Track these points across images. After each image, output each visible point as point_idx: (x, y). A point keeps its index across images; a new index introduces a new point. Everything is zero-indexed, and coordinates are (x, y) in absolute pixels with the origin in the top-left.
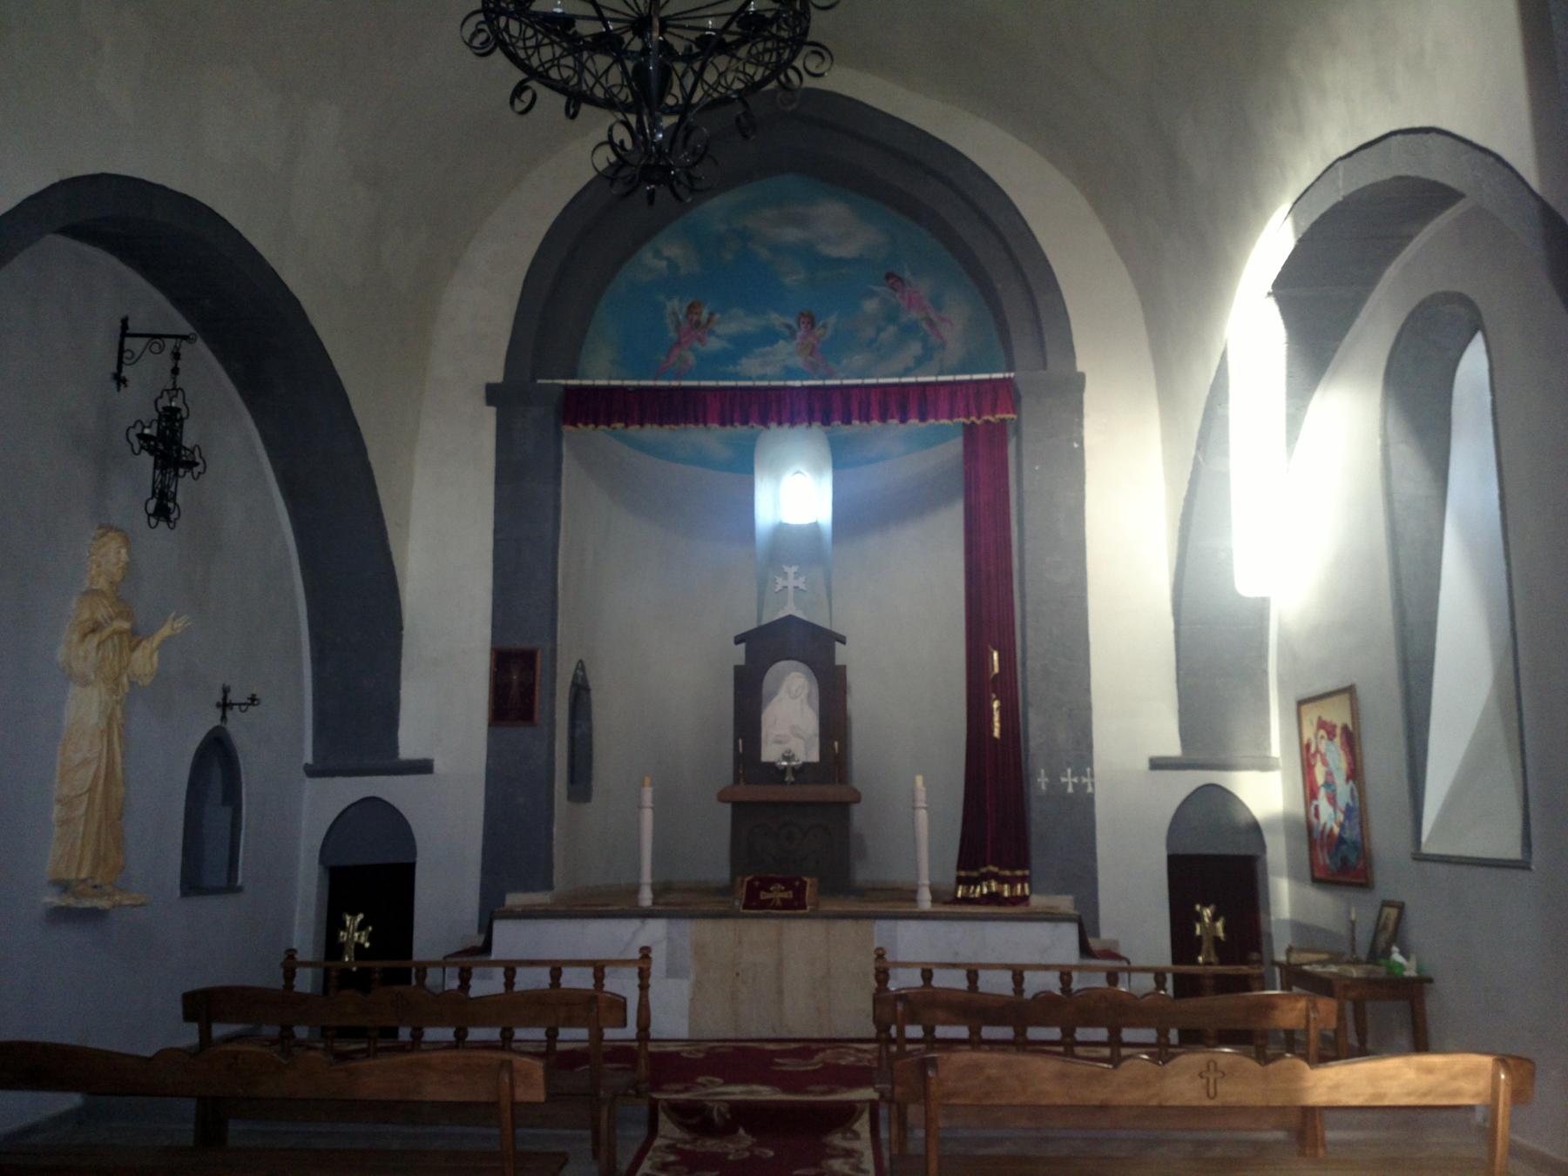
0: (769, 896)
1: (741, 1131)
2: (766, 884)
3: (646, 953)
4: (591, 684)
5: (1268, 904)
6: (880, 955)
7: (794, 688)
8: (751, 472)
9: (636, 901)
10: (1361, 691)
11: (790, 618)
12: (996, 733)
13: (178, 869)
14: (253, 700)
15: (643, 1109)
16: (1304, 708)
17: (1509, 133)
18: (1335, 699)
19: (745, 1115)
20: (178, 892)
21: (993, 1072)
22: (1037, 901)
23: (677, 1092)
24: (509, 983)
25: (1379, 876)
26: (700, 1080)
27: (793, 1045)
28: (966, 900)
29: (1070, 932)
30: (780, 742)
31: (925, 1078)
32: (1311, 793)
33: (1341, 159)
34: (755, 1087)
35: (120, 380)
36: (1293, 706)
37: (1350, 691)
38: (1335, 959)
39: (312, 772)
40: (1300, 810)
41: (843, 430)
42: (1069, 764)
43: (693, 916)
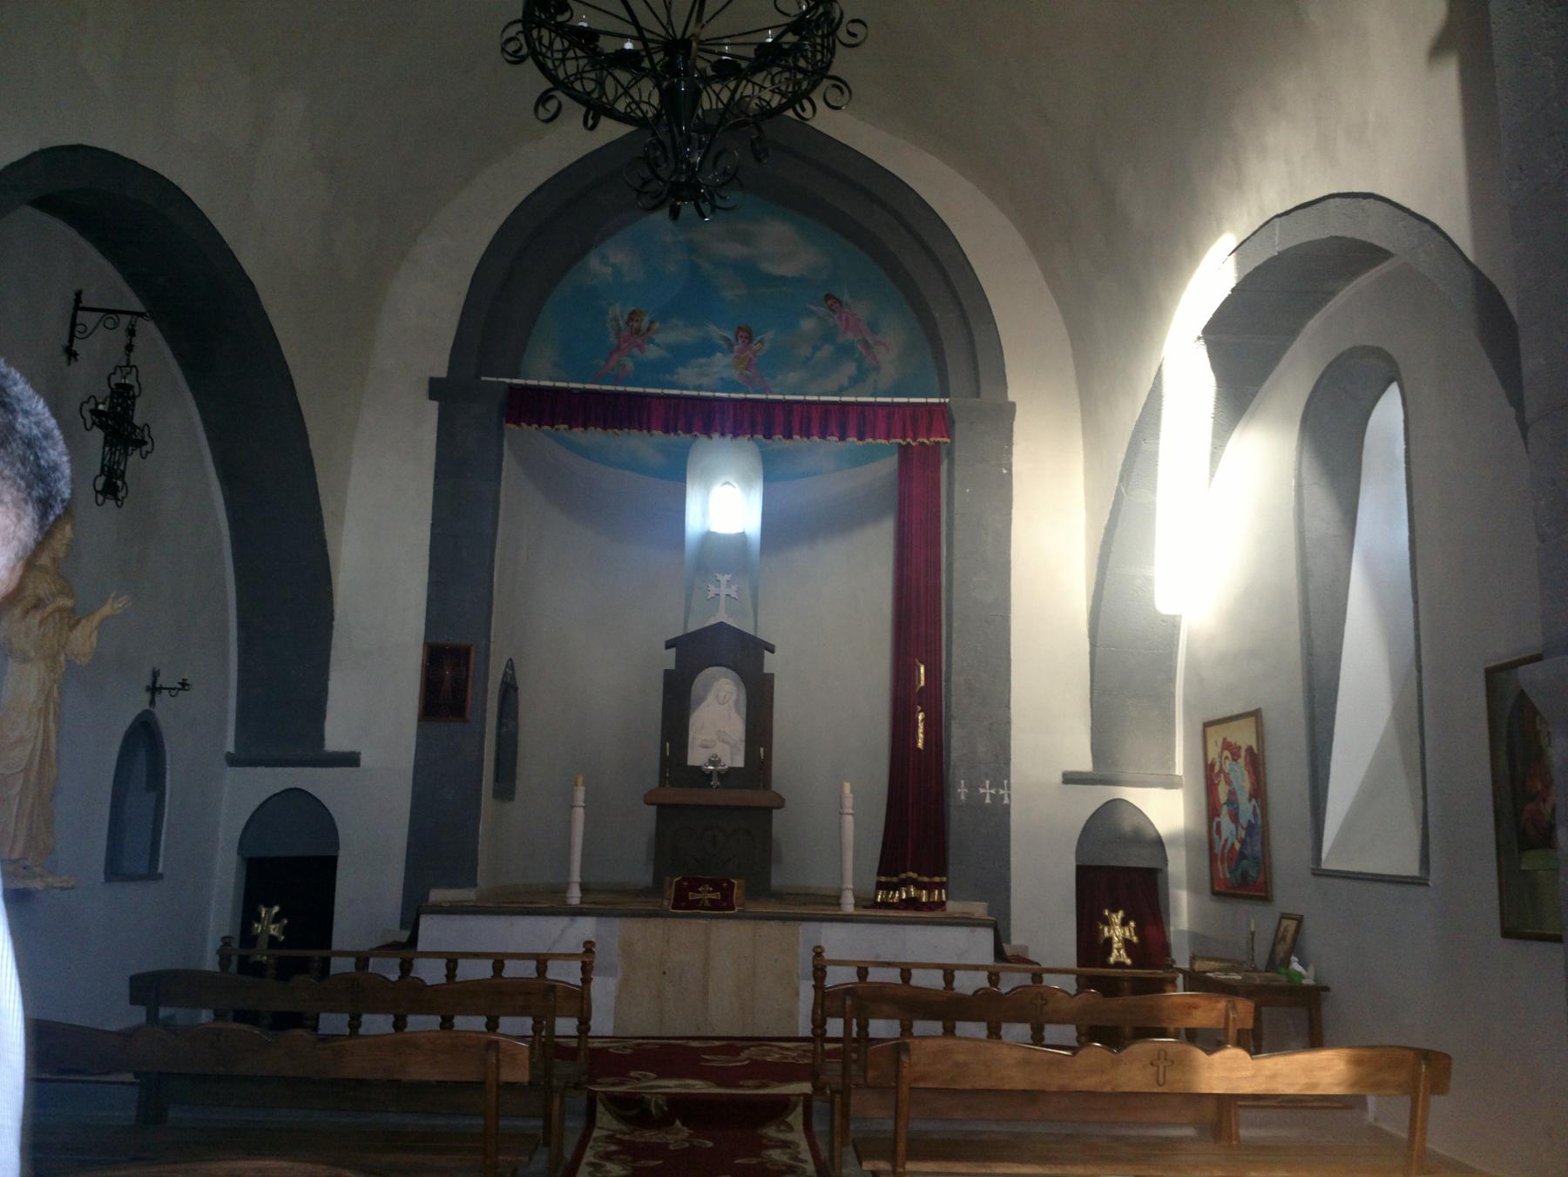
0: (698, 896)
1: (678, 1123)
2: (695, 885)
3: (589, 947)
6: (818, 952)
7: (722, 694)
8: (683, 480)
9: (564, 901)
10: (1267, 716)
11: (721, 626)
12: (920, 745)
13: (104, 849)
14: (184, 685)
15: (580, 1101)
16: (1209, 730)
17: (1450, 211)
18: (1242, 722)
19: (681, 1107)
21: (961, 1058)
22: (953, 907)
23: (613, 1085)
24: (451, 975)
25: (1277, 893)
27: (717, 1043)
28: (885, 905)
29: (986, 937)
31: (898, 1062)
32: (1213, 811)
33: (1278, 216)
35: (71, 354)
36: (1200, 728)
37: (1256, 715)
39: (233, 761)
41: (779, 442)
43: (621, 915)
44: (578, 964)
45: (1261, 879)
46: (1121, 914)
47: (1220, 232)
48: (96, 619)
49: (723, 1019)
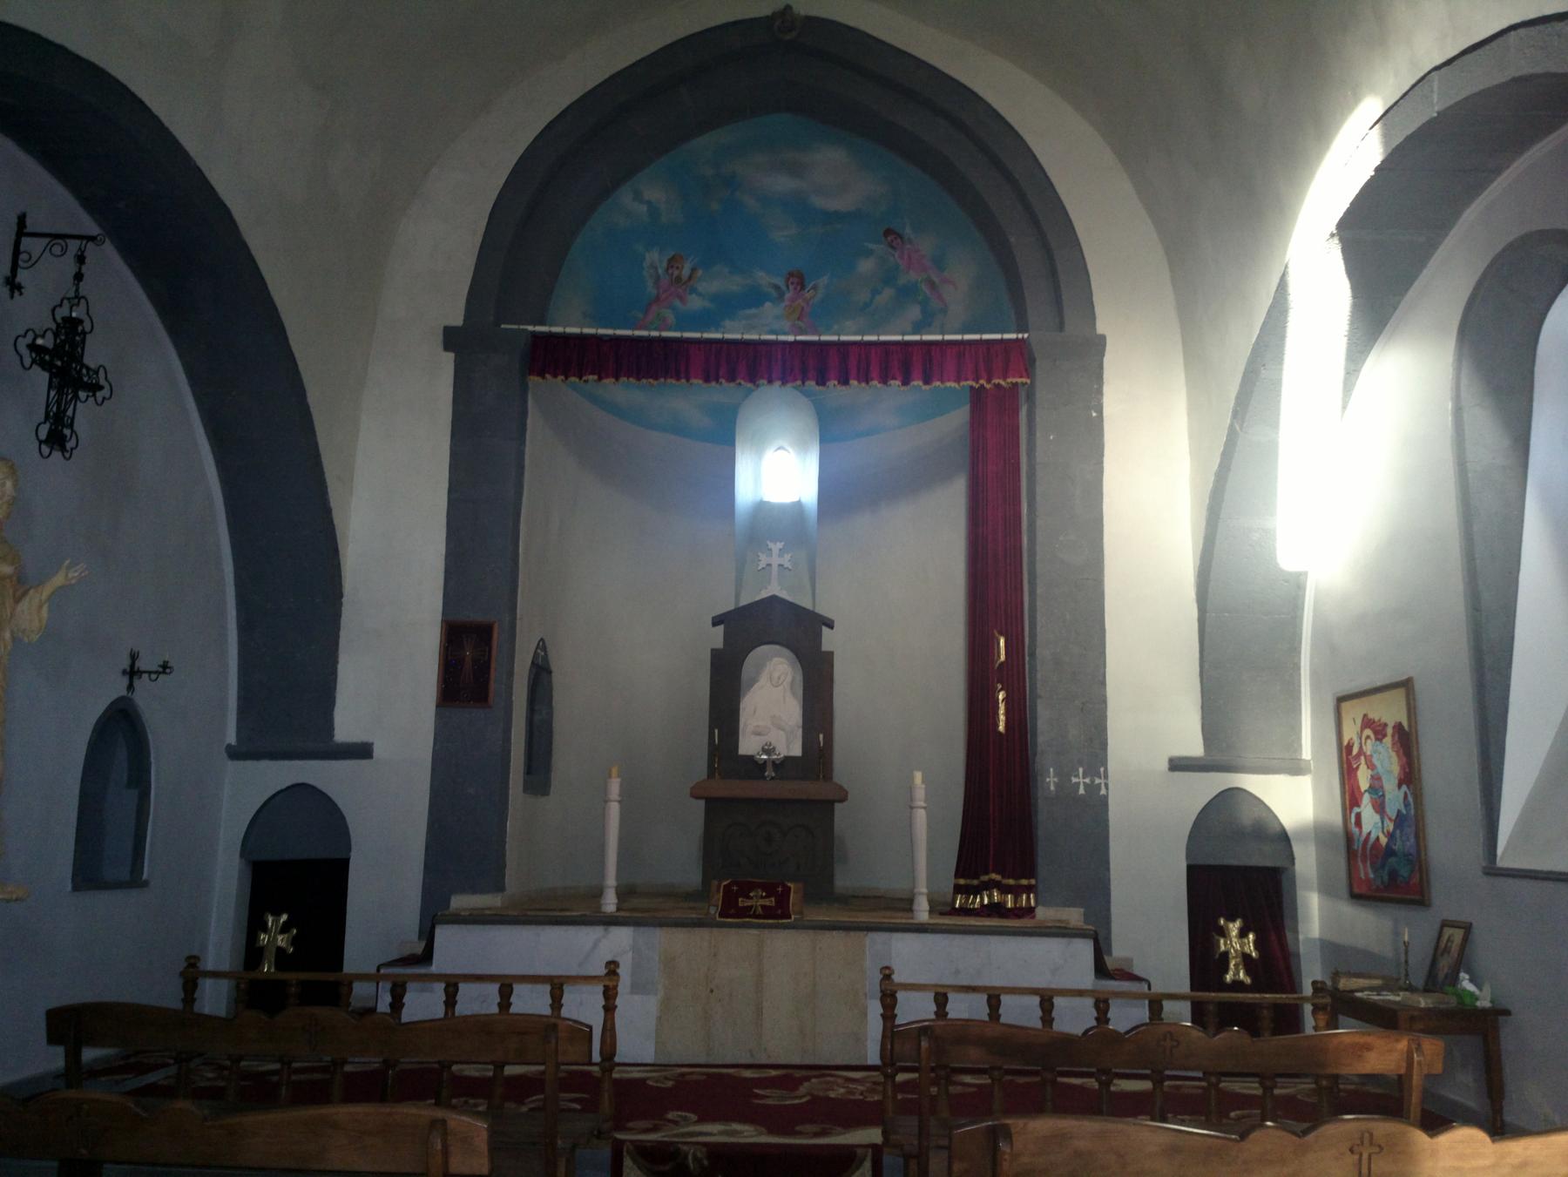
0: (748, 903)
2: (746, 889)
3: (612, 968)
4: (554, 668)
5: (1295, 918)
6: (887, 974)
7: (776, 675)
8: (733, 445)
11: (774, 598)
12: (1001, 728)
14: (165, 668)
15: (606, 1152)
16: (1345, 705)
20: (69, 888)
22: (1041, 913)
26: (671, 1115)
27: (773, 1073)
28: (965, 911)
29: (1084, 950)
30: (759, 734)
31: (995, 1150)
32: (1351, 798)
34: (736, 1126)
37: (1406, 685)
38: (1390, 985)
39: (234, 754)
40: (1336, 817)
42: (1080, 763)
43: (661, 924)
44: (600, 989)
45: (1416, 880)
46: (1238, 924)
47: (1357, 100)
48: (47, 590)
49: (780, 1044)
